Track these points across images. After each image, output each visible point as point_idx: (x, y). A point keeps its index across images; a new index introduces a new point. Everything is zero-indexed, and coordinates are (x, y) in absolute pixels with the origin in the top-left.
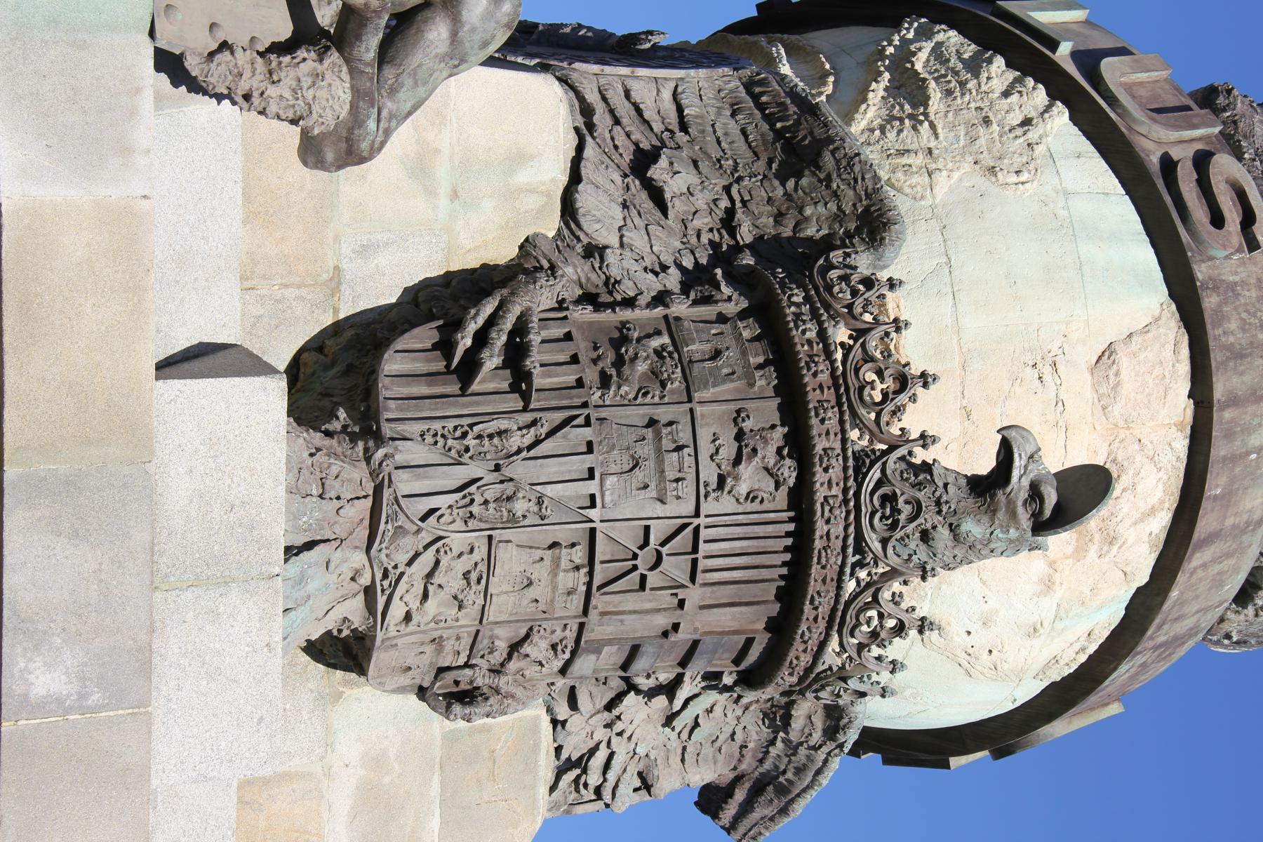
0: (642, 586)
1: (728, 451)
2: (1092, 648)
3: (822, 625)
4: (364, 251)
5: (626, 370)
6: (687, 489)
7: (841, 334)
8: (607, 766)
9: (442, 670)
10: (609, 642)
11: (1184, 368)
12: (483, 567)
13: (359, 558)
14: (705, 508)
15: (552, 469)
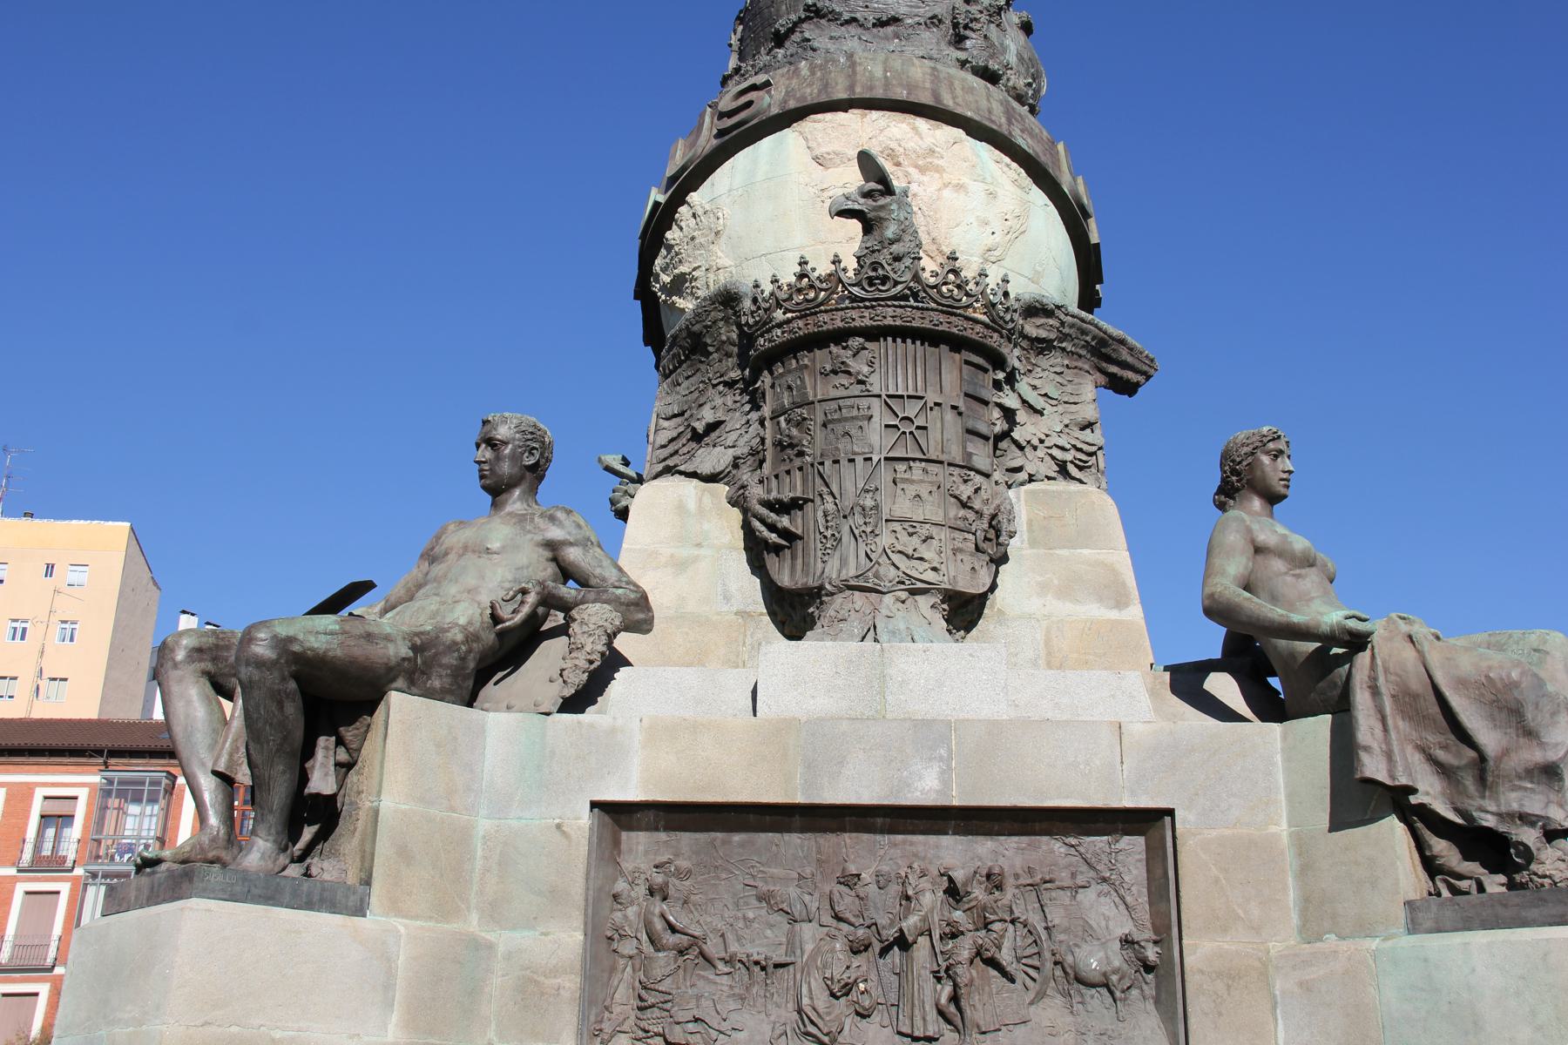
0: (925, 428)
1: (844, 380)
2: (1007, 160)
3: (953, 319)
4: (727, 598)
5: (795, 441)
6: (864, 402)
7: (779, 315)
8: (1063, 449)
9: (977, 549)
10: (964, 448)
11: (828, 116)
12: (906, 525)
13: (888, 599)
14: (876, 391)
15: (849, 486)
